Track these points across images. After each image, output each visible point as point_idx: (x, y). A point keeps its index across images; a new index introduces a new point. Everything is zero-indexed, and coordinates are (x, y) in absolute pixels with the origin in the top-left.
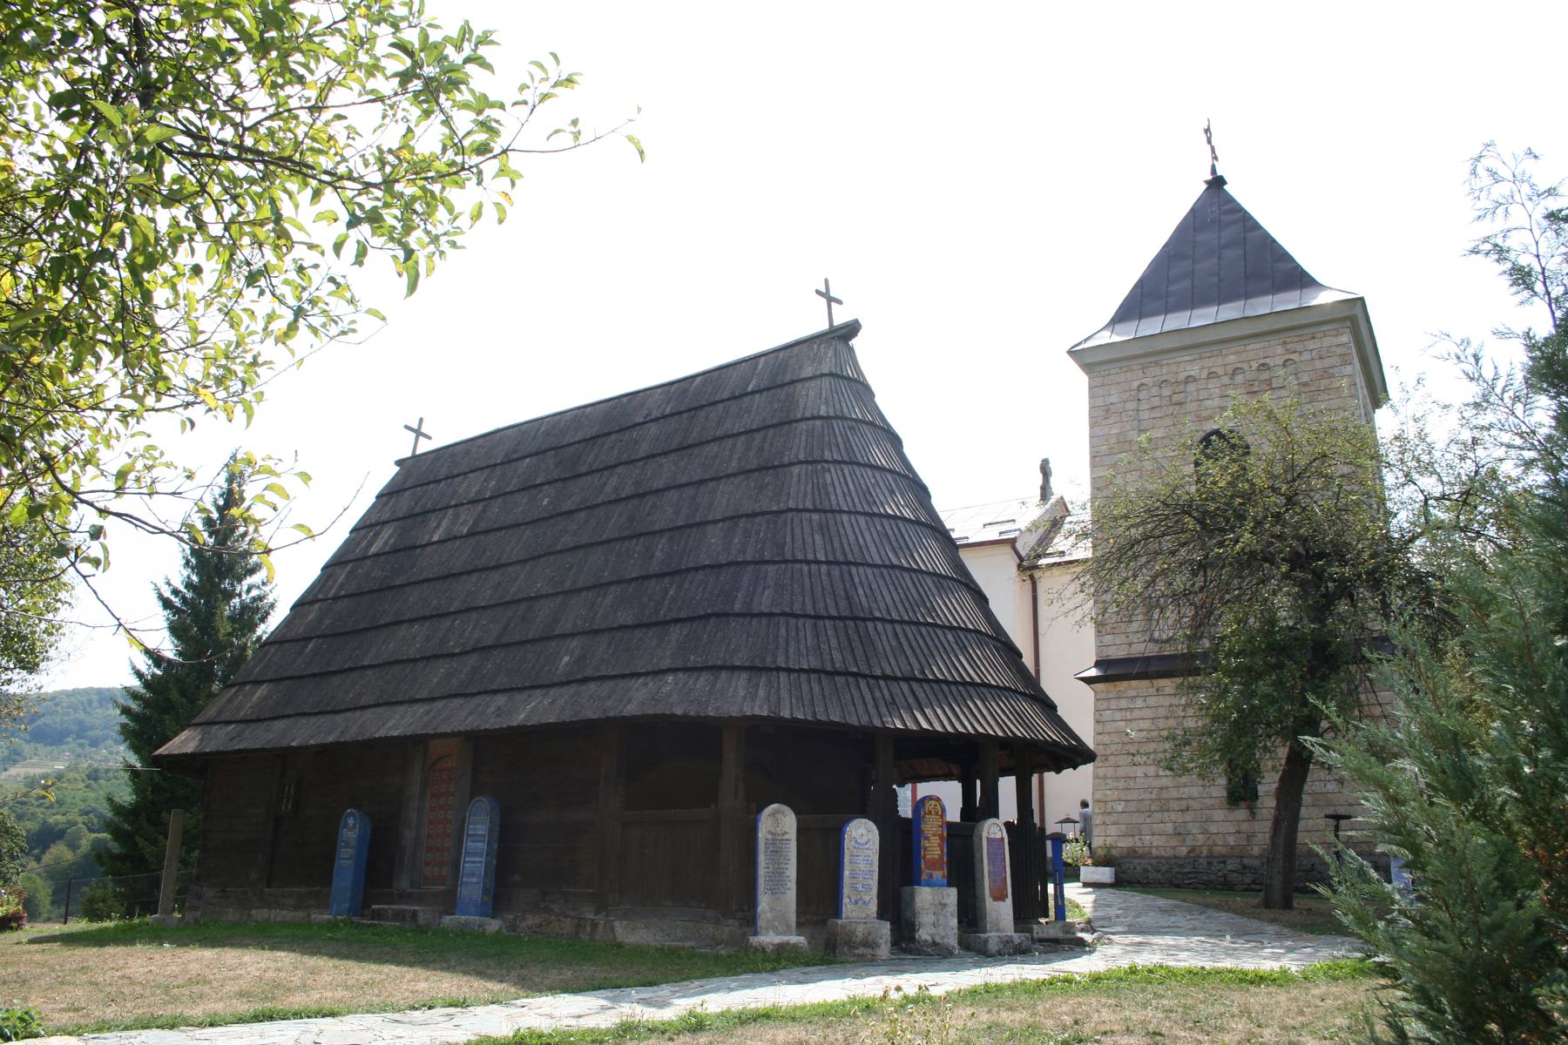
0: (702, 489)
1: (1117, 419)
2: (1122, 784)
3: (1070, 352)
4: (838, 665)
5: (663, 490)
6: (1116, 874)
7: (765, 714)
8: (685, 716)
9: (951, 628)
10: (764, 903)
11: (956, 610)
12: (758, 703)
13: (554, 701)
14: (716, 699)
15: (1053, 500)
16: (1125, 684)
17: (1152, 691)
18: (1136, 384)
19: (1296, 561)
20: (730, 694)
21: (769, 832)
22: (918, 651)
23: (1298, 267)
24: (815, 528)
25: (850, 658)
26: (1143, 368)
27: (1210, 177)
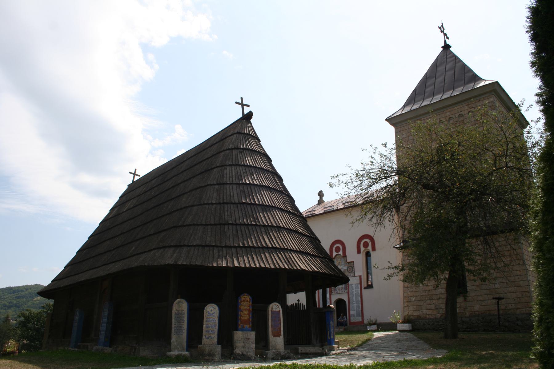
6: (412, 326)
10: (174, 339)
21: (176, 310)
27: (443, 45)
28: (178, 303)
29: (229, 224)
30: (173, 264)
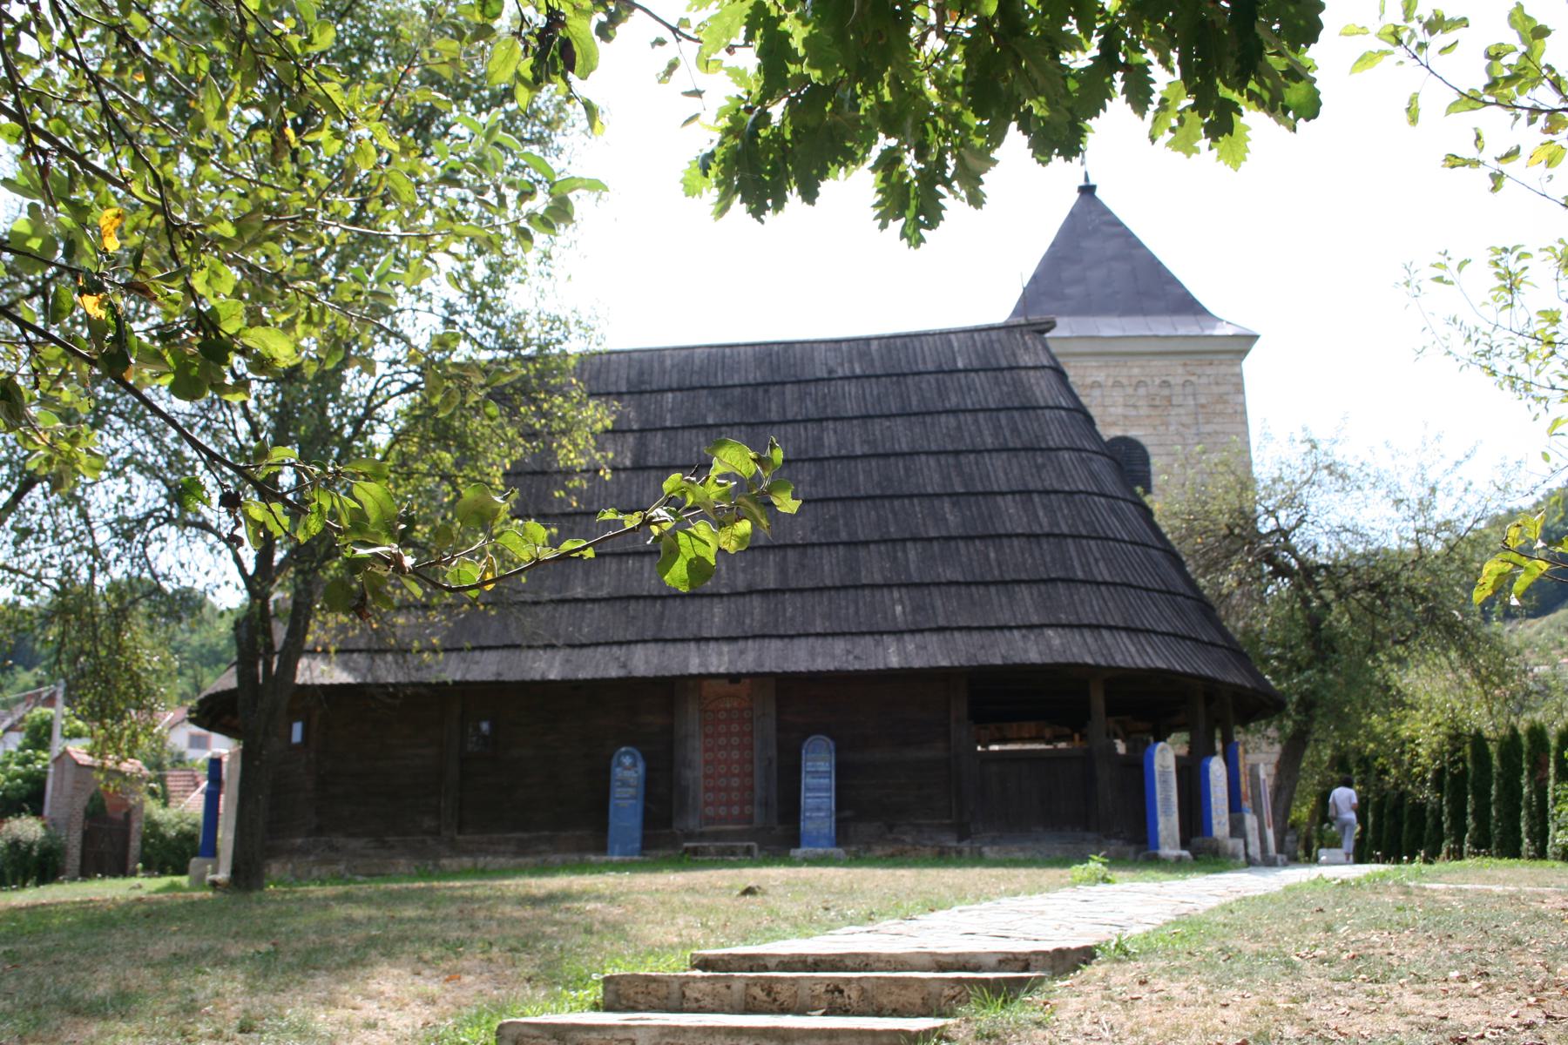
23: (1187, 294)
27: (1082, 183)
28: (1163, 750)
30: (760, 54)
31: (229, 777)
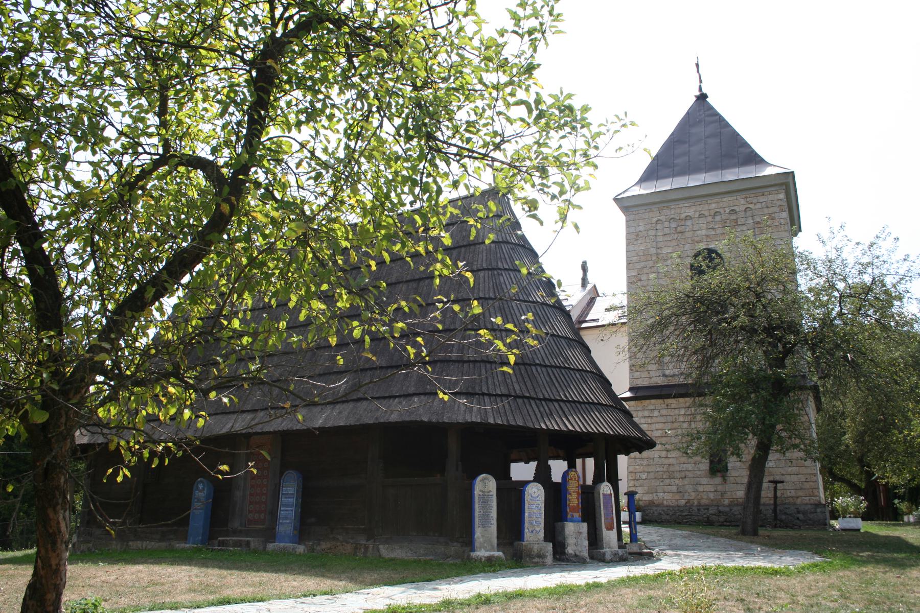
0: (421, 283)
1: (643, 241)
2: (645, 462)
3: (615, 199)
4: (518, 392)
5: (395, 283)
7: (479, 421)
8: (430, 422)
9: (578, 370)
10: (478, 533)
11: (576, 359)
12: (474, 414)
13: (340, 413)
14: (448, 412)
15: (589, 287)
16: (648, 401)
17: (664, 406)
18: (655, 220)
19: (769, 330)
20: (456, 409)
21: (480, 491)
22: (562, 384)
23: (753, 151)
24: (497, 309)
25: (523, 387)
26: (660, 210)
27: (698, 93)
29: (536, 365)
31: (625, 429)
